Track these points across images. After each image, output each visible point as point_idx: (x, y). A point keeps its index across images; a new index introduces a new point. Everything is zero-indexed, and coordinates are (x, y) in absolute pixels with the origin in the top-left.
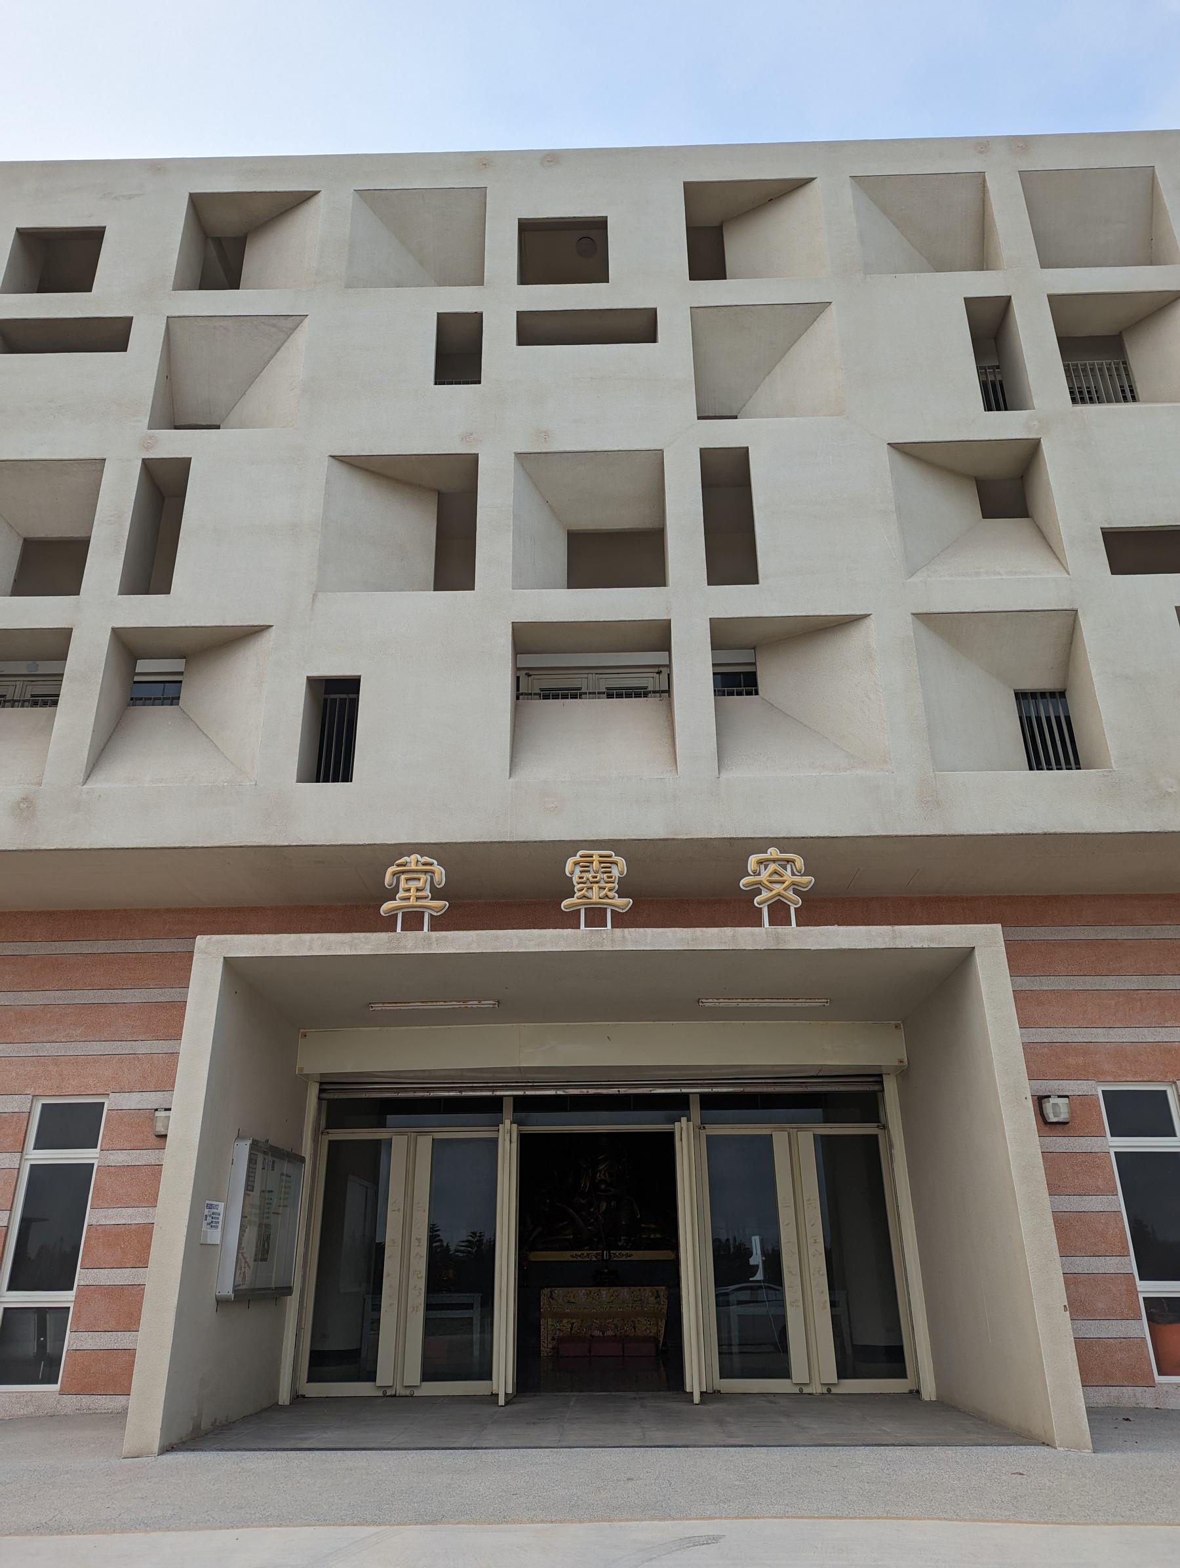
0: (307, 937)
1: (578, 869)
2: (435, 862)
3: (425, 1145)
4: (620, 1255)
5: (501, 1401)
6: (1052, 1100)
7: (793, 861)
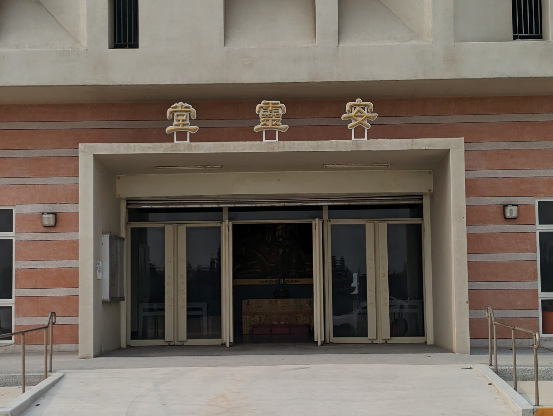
0: (132, 145)
1: (262, 110)
2: (191, 106)
3: (182, 230)
4: (291, 281)
5: (228, 345)
6: (509, 208)
7: (368, 106)
